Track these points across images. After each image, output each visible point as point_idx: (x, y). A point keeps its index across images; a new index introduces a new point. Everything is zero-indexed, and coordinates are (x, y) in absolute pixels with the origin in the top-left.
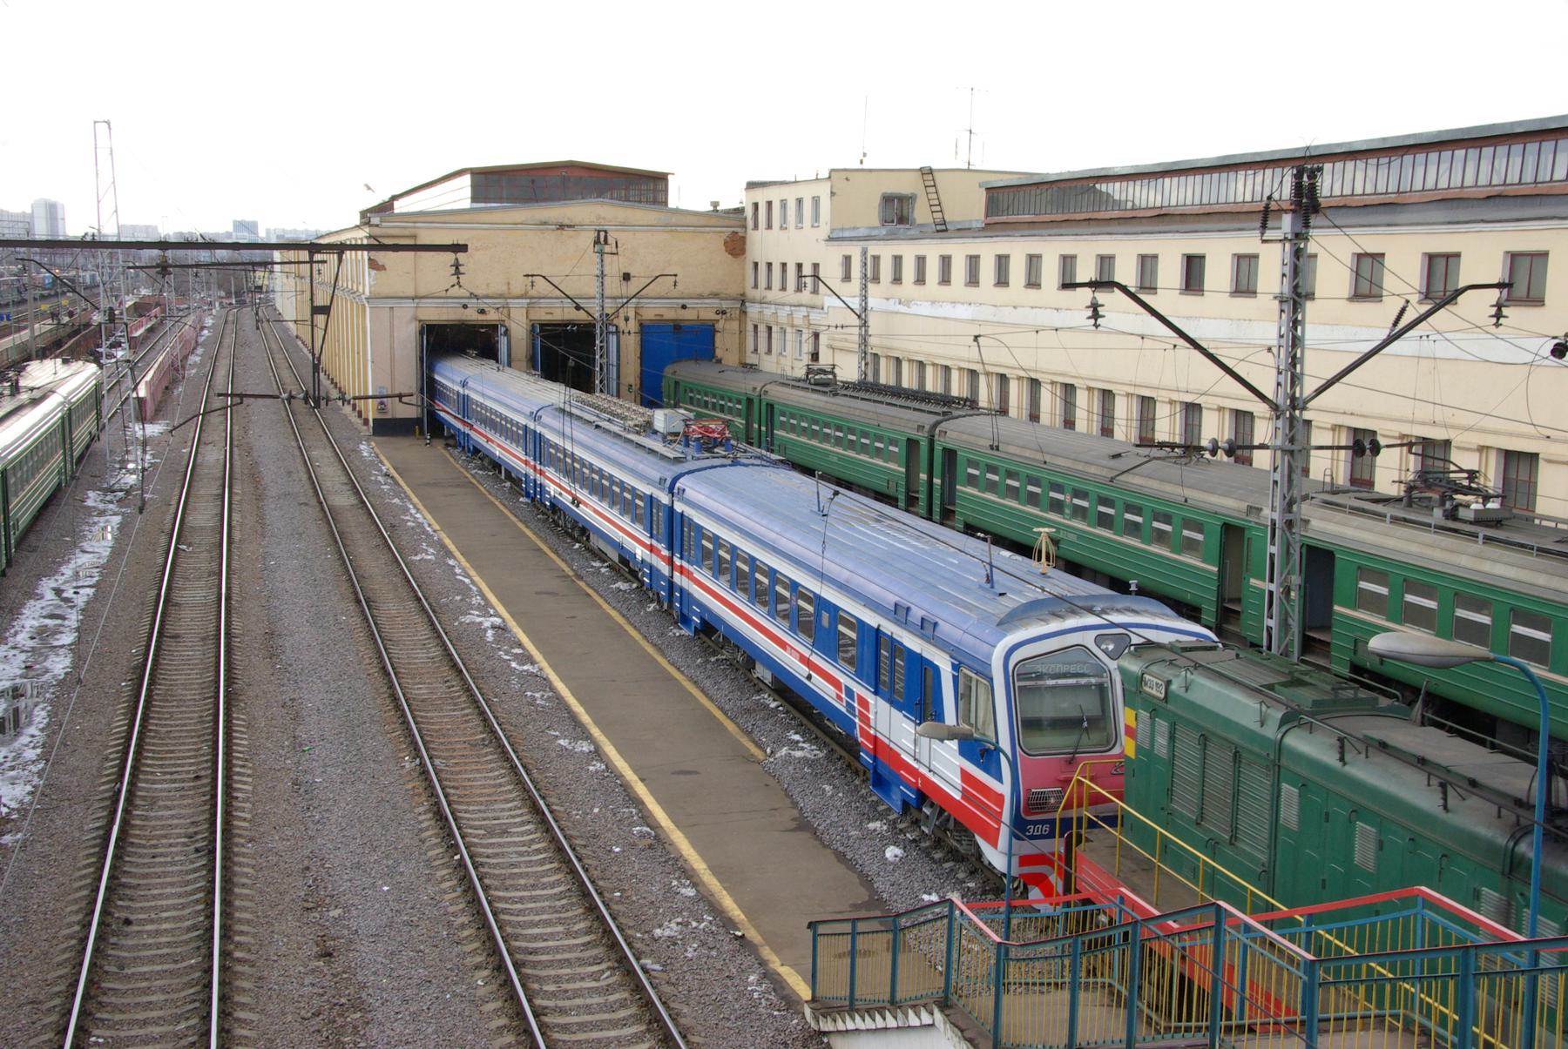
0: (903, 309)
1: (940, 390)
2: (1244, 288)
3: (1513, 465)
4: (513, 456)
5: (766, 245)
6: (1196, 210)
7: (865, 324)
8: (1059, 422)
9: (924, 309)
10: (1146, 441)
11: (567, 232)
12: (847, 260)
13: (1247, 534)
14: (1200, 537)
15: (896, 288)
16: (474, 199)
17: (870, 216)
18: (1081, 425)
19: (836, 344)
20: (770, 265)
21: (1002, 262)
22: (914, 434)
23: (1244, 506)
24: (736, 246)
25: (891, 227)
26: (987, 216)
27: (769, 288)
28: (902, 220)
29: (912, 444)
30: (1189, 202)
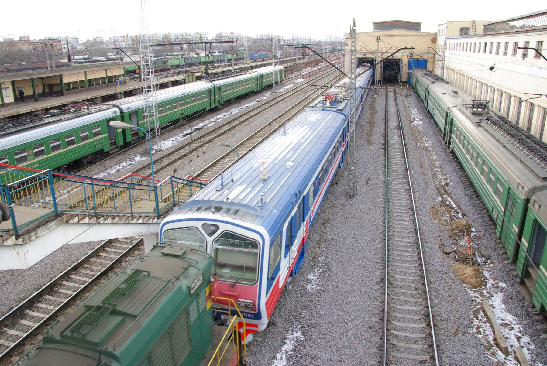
11: (392, 37)
16: (374, 29)
25: (463, 36)
28: (466, 34)
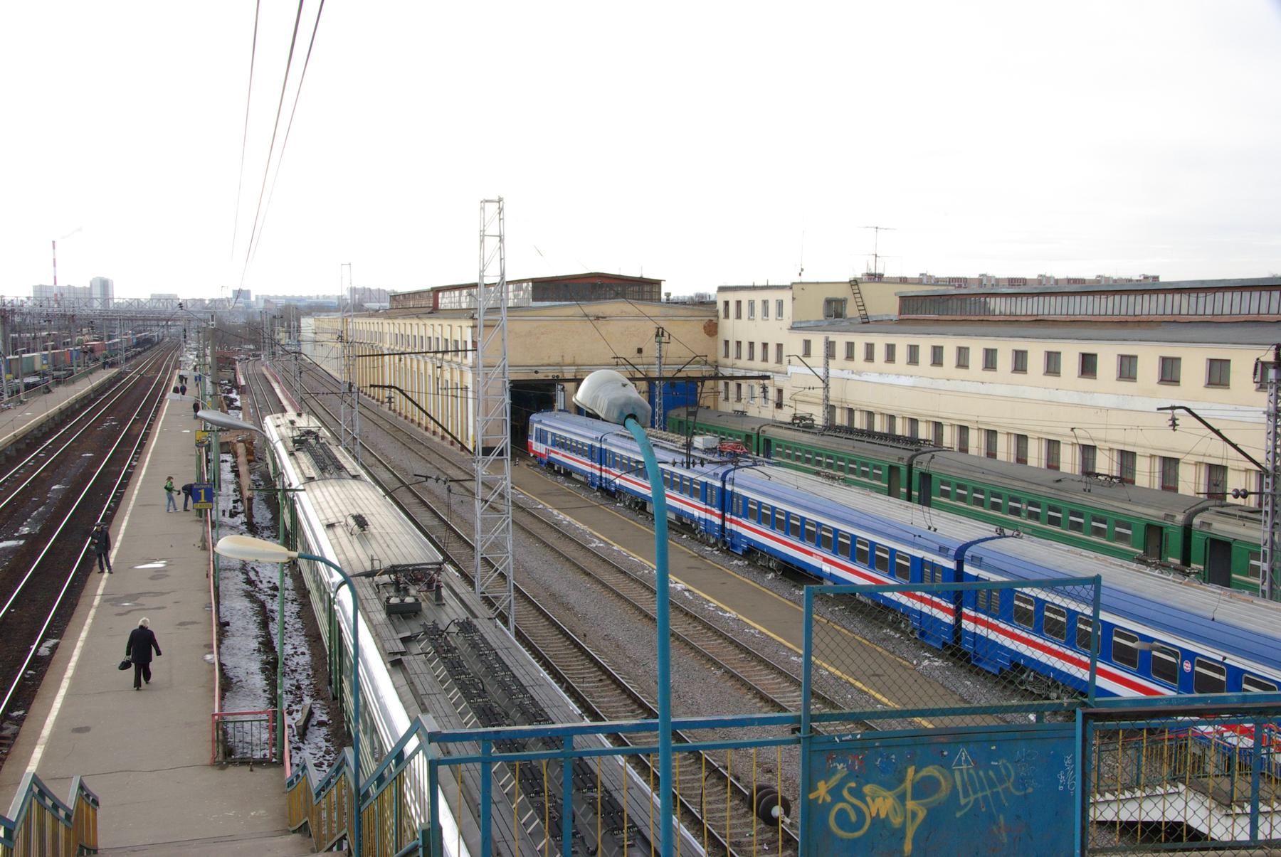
0: (855, 377)
1: (846, 423)
2: (1168, 378)
3: (1214, 473)
4: (582, 464)
5: (732, 329)
6: (1063, 318)
7: (827, 387)
8: (983, 453)
9: (874, 378)
10: (1088, 471)
12: (807, 344)
13: (1165, 531)
14: (1129, 532)
15: (849, 363)
17: (818, 313)
18: (973, 450)
19: (797, 398)
20: (739, 343)
21: (850, 346)
22: (894, 462)
23: (1162, 514)
24: (712, 329)
26: (900, 314)
27: (739, 357)
28: (839, 315)
29: (893, 470)
30: (1176, 311)
